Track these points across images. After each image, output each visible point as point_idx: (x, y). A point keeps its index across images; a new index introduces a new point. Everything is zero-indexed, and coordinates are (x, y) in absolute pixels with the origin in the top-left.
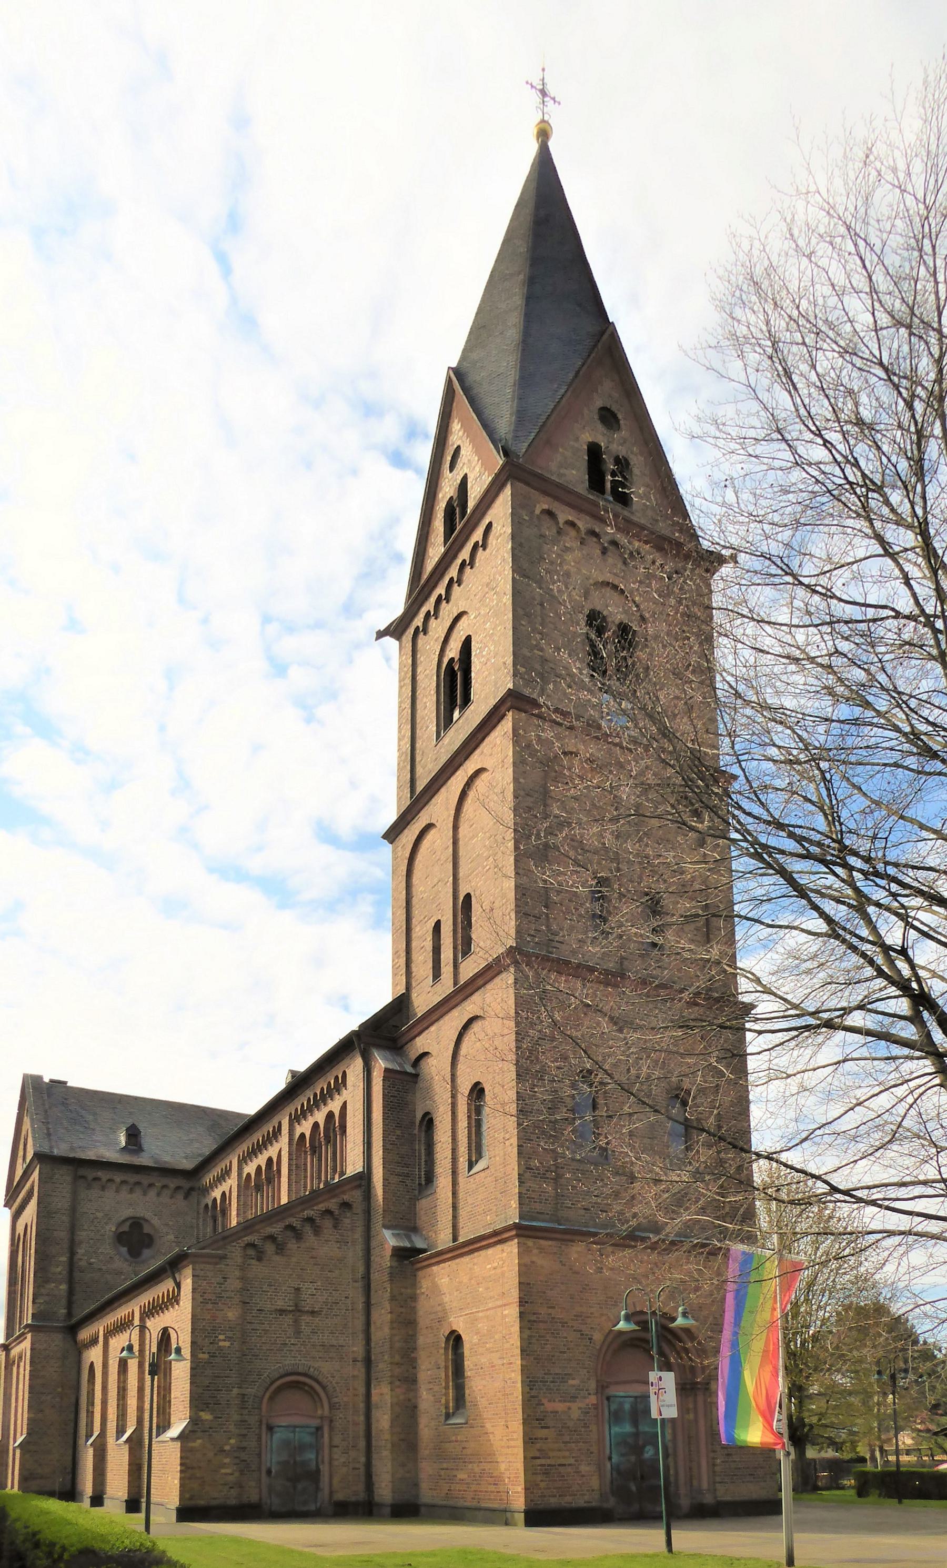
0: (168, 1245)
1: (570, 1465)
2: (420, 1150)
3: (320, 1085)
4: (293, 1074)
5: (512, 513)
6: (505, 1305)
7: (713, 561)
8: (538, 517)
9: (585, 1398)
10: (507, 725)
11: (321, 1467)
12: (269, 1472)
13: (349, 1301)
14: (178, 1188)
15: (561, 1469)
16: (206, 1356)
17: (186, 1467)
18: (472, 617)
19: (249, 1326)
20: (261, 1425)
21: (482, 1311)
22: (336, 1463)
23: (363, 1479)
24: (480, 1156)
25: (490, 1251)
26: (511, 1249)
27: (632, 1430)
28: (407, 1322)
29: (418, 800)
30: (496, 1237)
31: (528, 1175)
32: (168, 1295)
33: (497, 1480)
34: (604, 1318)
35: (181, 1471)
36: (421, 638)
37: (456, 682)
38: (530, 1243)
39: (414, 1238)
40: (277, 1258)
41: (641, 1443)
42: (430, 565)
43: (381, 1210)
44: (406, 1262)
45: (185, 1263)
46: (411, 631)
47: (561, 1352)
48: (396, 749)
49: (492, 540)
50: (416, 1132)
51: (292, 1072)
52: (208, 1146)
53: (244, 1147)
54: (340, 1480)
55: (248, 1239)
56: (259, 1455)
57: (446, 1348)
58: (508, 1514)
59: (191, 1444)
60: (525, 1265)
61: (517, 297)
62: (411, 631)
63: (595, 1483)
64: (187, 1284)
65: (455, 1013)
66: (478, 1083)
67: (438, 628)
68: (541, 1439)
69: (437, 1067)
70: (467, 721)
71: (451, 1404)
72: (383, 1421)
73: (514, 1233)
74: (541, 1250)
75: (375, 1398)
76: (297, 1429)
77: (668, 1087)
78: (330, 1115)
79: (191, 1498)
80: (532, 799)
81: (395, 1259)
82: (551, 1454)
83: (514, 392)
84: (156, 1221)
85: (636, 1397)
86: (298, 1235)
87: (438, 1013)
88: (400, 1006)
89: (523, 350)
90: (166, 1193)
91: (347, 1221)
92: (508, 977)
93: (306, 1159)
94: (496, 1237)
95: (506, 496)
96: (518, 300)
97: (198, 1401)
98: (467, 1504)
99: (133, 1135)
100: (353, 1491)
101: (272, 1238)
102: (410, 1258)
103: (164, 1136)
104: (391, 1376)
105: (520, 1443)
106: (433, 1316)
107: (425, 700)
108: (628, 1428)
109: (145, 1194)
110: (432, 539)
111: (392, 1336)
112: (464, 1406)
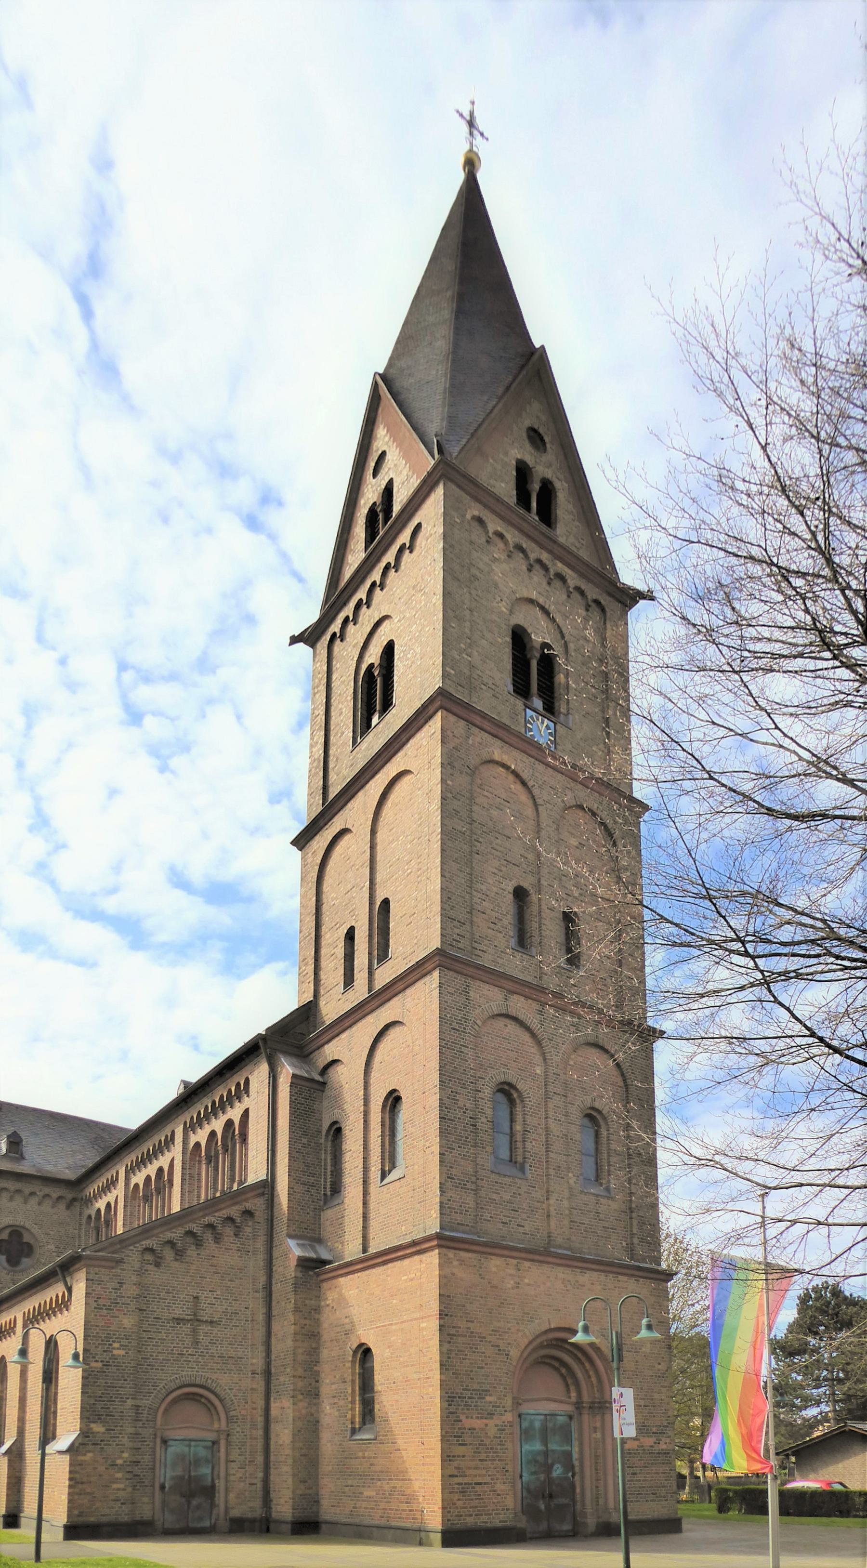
0: (48, 1257)
1: (485, 1483)
2: (325, 1159)
3: (220, 1092)
4: (186, 1084)
5: (444, 512)
6: (422, 1318)
7: (630, 597)
8: (469, 522)
9: (502, 1415)
10: (435, 725)
11: (217, 1481)
12: (162, 1487)
13: (248, 1312)
14: (60, 1198)
15: (478, 1488)
16: (99, 1365)
17: (75, 1481)
18: (396, 621)
19: (144, 1334)
20: (155, 1438)
21: (396, 1324)
22: (232, 1478)
23: (260, 1494)
24: (393, 1166)
25: (406, 1262)
26: (433, 1258)
27: (544, 1448)
28: (311, 1336)
29: (331, 806)
30: (416, 1247)
31: (449, 1184)
32: (57, 1300)
33: (410, 1499)
34: (520, 1334)
35: (70, 1487)
36: (338, 645)
37: (375, 689)
38: (451, 1254)
39: (318, 1247)
40: (176, 1264)
41: (550, 1462)
42: (348, 573)
43: (285, 1220)
44: (311, 1273)
45: (77, 1266)
46: (327, 637)
47: (478, 1368)
48: (309, 755)
49: (420, 540)
50: (322, 1141)
51: (184, 1082)
52: (91, 1159)
53: (130, 1158)
54: (237, 1495)
55: (146, 1243)
56: (153, 1469)
57: (353, 1362)
58: (423, 1534)
59: (81, 1458)
60: (445, 1277)
61: (446, 312)
62: (327, 637)
63: (510, 1502)
64: (80, 1288)
65: (370, 1019)
66: (394, 1091)
67: (356, 634)
68: (459, 1456)
69: (347, 1078)
70: (386, 726)
71: (357, 1420)
72: (283, 1435)
73: (435, 1243)
74: (462, 1262)
75: (274, 1412)
76: (193, 1443)
77: (582, 1106)
78: (229, 1123)
79: (81, 1514)
80: (460, 803)
81: (300, 1269)
82: (468, 1472)
83: (445, 398)
84: (35, 1230)
85: (546, 1415)
86: (199, 1243)
87: (400, 985)
88: (307, 1013)
89: (453, 360)
90: (48, 1203)
91: (248, 1230)
92: (434, 979)
93: (200, 1169)
94: (416, 1247)
95: (438, 494)
96: (447, 313)
97: (90, 1411)
98: (376, 1522)
99: (15, 1143)
100: (252, 1508)
101: (171, 1243)
102: (314, 1268)
103: (46, 1146)
104: (294, 1390)
105: (438, 1460)
106: (339, 1329)
107: (340, 706)
108: (538, 1446)
109: (26, 1202)
110: (352, 545)
111: (295, 1348)
112: (373, 1420)
